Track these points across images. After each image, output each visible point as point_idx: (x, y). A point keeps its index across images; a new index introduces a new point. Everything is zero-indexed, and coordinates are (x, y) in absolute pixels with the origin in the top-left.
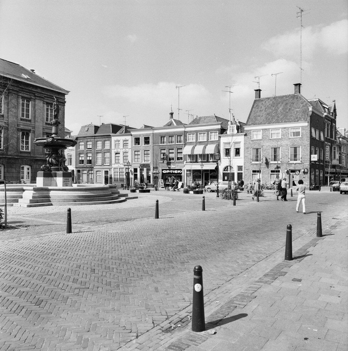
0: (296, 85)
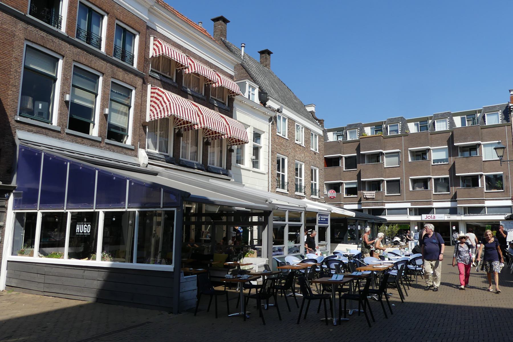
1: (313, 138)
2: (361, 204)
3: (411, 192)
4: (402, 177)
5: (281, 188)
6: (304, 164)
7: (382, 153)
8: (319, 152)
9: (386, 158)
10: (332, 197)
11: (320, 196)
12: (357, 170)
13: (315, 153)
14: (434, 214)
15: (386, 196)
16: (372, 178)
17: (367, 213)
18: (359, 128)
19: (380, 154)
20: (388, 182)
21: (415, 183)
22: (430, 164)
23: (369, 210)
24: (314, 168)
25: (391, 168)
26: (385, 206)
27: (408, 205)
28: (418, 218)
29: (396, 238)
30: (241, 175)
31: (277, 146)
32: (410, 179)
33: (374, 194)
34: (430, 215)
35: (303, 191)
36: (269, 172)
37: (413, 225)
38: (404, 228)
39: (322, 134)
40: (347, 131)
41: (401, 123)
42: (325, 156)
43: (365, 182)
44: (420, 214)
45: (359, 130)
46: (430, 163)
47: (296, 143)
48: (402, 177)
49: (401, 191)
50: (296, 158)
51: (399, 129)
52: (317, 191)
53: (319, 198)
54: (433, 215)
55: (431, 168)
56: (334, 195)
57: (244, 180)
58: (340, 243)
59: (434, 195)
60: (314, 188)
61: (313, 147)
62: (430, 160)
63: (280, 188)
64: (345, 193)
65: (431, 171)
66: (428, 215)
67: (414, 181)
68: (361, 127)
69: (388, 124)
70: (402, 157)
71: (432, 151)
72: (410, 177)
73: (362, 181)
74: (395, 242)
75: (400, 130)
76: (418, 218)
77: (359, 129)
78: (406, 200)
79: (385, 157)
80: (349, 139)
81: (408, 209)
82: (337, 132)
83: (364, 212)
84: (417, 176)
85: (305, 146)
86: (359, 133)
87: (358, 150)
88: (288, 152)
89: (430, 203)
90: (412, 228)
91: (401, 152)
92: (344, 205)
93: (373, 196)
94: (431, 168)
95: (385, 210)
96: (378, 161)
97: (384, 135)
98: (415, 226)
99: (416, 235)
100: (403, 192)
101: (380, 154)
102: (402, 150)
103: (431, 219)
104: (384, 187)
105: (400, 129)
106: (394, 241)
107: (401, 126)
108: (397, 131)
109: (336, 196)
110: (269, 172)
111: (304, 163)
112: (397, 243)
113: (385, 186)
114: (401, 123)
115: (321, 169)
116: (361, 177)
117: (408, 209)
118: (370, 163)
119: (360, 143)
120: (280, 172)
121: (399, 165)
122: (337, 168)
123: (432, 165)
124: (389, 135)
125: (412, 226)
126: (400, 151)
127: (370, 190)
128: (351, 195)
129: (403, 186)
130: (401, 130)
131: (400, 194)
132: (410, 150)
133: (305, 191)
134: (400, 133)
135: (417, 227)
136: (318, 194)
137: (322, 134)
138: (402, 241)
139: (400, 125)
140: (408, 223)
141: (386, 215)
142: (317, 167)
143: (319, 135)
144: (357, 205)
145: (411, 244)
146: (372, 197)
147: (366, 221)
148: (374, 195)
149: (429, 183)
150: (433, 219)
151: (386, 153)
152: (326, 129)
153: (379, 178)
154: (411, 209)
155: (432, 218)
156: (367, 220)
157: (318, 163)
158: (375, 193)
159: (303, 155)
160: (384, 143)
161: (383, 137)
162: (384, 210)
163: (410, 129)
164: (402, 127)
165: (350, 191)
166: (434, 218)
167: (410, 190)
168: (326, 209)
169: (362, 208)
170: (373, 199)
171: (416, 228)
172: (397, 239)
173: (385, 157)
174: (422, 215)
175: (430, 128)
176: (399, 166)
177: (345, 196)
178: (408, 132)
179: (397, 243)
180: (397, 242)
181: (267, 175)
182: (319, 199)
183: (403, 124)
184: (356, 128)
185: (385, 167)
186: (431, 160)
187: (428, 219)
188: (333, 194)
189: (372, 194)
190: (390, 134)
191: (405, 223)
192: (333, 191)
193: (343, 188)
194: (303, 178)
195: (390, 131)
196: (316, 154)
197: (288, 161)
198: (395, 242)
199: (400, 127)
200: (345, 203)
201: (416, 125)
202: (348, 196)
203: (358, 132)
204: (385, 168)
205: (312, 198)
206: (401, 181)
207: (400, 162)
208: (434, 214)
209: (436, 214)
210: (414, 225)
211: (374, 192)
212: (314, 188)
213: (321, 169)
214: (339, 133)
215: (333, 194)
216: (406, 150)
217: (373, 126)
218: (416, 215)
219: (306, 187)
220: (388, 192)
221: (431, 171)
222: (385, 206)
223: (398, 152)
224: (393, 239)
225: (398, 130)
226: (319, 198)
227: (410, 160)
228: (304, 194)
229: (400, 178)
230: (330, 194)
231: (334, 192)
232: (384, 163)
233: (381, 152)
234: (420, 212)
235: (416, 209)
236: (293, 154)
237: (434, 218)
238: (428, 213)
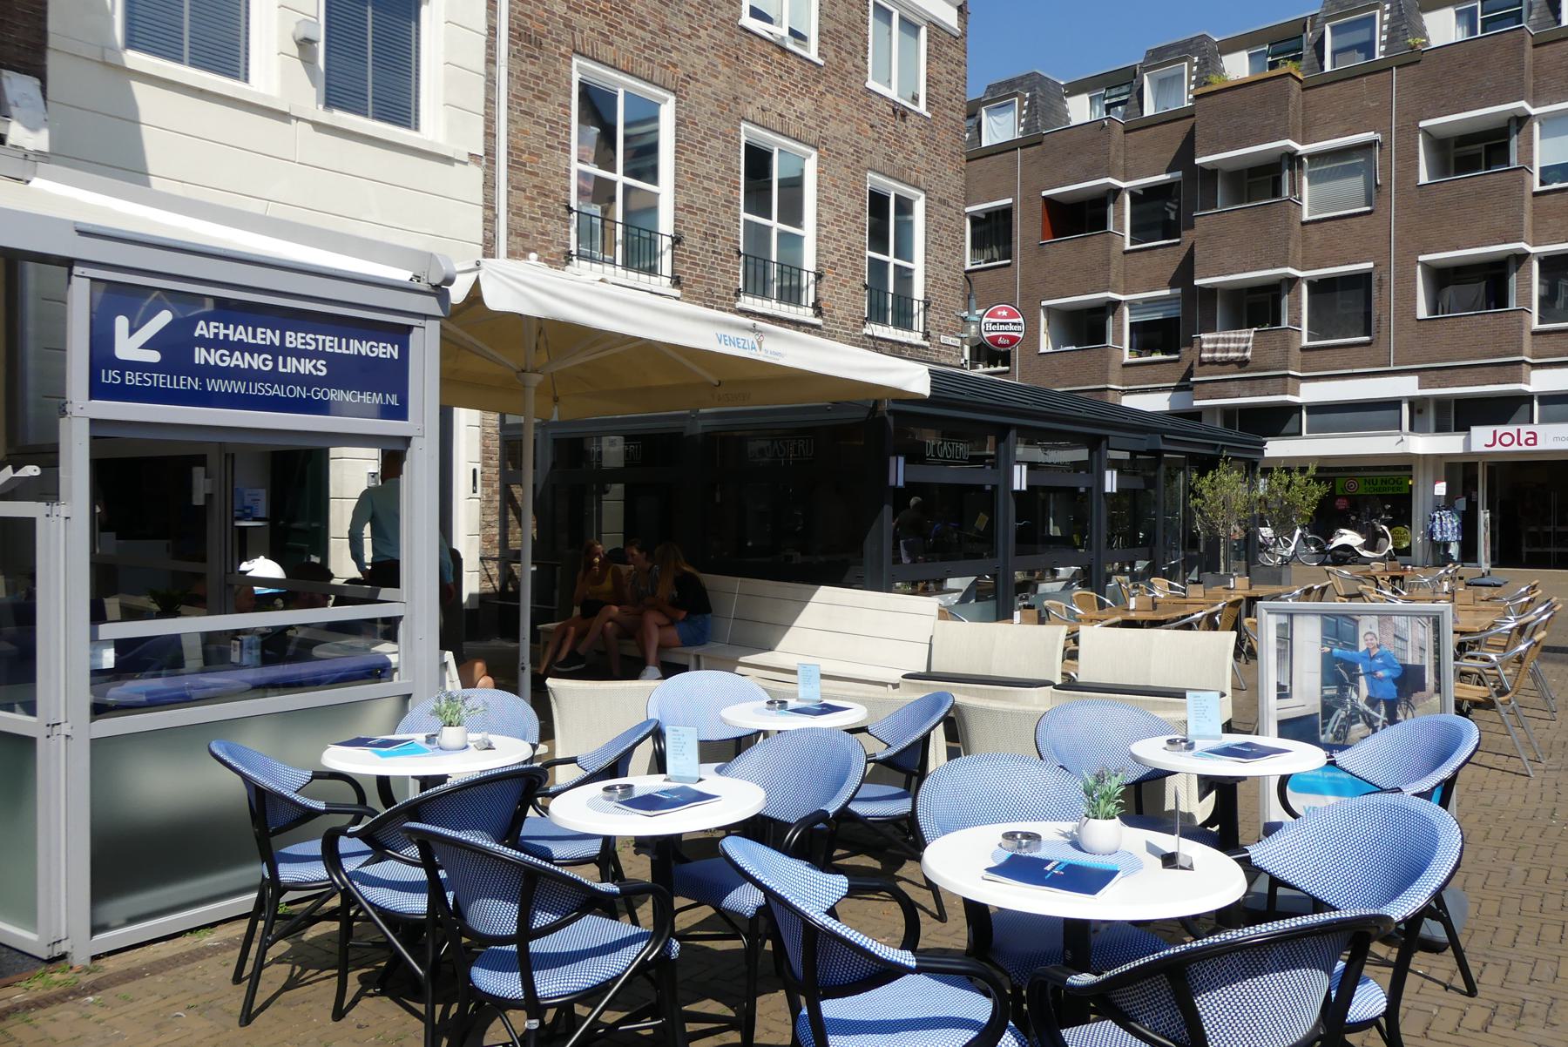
1: (890, 33)
2: (1192, 389)
3: (1422, 323)
4: (1382, 262)
5: (619, 261)
6: (814, 154)
7: (1292, 159)
8: (928, 109)
9: (1310, 183)
10: (1000, 341)
11: (932, 333)
12: (1178, 244)
13: (901, 113)
14: (1531, 421)
15: (1303, 350)
16: (1245, 272)
17: (1219, 424)
18: (1196, 59)
19: (1286, 163)
20: (1317, 287)
21: (1447, 285)
22: (1522, 183)
23: (1228, 412)
24: (893, 188)
25: (1333, 223)
26: (1296, 394)
27: (1407, 386)
28: (1450, 444)
29: (1342, 535)
30: (137, 122)
31: (570, 13)
32: (1419, 267)
33: (1248, 340)
34: (1512, 429)
35: (809, 296)
36: (490, 153)
37: (1425, 476)
38: (1384, 489)
39: (956, 27)
40: (1145, 75)
41: (1388, 7)
42: (1045, 193)
43: (1210, 292)
44: (1463, 427)
45: (1195, 68)
46: (1527, 181)
47: (747, 31)
48: (1382, 262)
49: (1374, 324)
50: (750, 111)
51: (1380, 38)
52: (917, 307)
53: (927, 344)
54: (1525, 428)
55: (1528, 204)
56: (1011, 328)
57: (157, 149)
58: (837, 578)
59: (1535, 333)
60: (1484, 516)
61: (889, 81)
62: (1525, 169)
63: (613, 263)
64: (1131, 347)
65: (1527, 219)
66: (1501, 429)
67: (1441, 277)
68: (1206, 53)
69: (1328, 19)
70: (1386, 168)
71: (1536, 126)
72: (1422, 258)
73: (1200, 288)
74: (1339, 553)
75: (1381, 43)
76: (1450, 444)
77: (1197, 64)
78: (1395, 365)
79: (1305, 180)
80: (1149, 110)
81: (1405, 408)
82: (1107, 89)
83: (1206, 421)
84: (1458, 248)
85: (820, 62)
86: (1194, 78)
87: (1188, 148)
88: (675, 66)
89: (1514, 370)
90: (1420, 489)
91: (1381, 145)
92: (1124, 398)
93: (1245, 350)
94: (1528, 204)
95: (1296, 416)
96: (1277, 192)
97: (1306, 72)
98: (1436, 482)
99: (1438, 521)
100: (1383, 330)
101: (1286, 163)
102: (1387, 133)
103: (1515, 447)
104: (1300, 309)
105: (1384, 38)
106: (1332, 547)
107: (1388, 22)
108: (1368, 48)
109: (1021, 335)
110: (490, 153)
111: (816, 147)
112: (1346, 558)
113: (1300, 304)
114: (1391, 8)
115: (943, 202)
116: (1197, 269)
117: (1405, 408)
118: (1242, 203)
119: (1193, 127)
120: (613, 170)
121: (1370, 205)
122: (1094, 241)
123: (1536, 194)
124: (1328, 68)
125: (1418, 484)
126: (1378, 136)
127: (1237, 326)
128: (1153, 351)
129: (1385, 303)
130: (1388, 43)
131: (1367, 338)
132: (1425, 131)
133: (817, 300)
134: (1381, 53)
135: (1444, 484)
136: (918, 322)
137: (956, 27)
138: (1371, 545)
139: (1387, 17)
140: (1404, 466)
141: (1300, 433)
142: (916, 186)
143: (930, 22)
144: (1168, 395)
145: (1286, 639)
146: (1241, 355)
147: (1099, 444)
148: (1250, 344)
149: (1513, 280)
150: (1525, 448)
151: (1312, 157)
152: (1062, 83)
153: (1274, 267)
154: (1417, 405)
155: (1522, 442)
156: (1107, 437)
157: (922, 164)
158: (1252, 335)
159: (805, 105)
160: (1304, 107)
161: (1300, 81)
162: (1290, 417)
163: (1429, 32)
164: (1394, 25)
165: (1150, 336)
166: (1531, 442)
167: (1419, 317)
168: (403, 276)
169: (1196, 403)
170: (1242, 364)
171: (1441, 489)
172: (1350, 538)
173: (1305, 180)
174: (1474, 429)
175: (1532, 17)
176: (1368, 208)
177: (1127, 357)
178: (1422, 44)
179: (1347, 558)
180: (1348, 554)
181: (476, 174)
182: (926, 348)
183: (1400, 10)
184: (1184, 59)
185: (1306, 217)
186: (1532, 167)
187: (1498, 448)
188: (1005, 324)
189: (1240, 340)
190: (1334, 65)
191: (1387, 468)
192: (1006, 309)
193: (1121, 325)
194: (809, 230)
195: (1334, 53)
196: (904, 116)
197: (677, 118)
198: (1339, 553)
199: (1385, 28)
200: (1126, 388)
201: (1465, 18)
202: (1140, 356)
203: (1190, 73)
204: (1304, 224)
205: (872, 337)
206: (1375, 278)
207: (1374, 192)
208: (1531, 421)
209: (1542, 421)
210: (1430, 478)
211: (1249, 334)
212: (1484, 516)
213: (943, 202)
214: (1114, 92)
215: (1005, 324)
216: (1408, 131)
217: (1263, 44)
218: (1441, 428)
219: (829, 276)
220: (1316, 329)
221: (1527, 219)
222: (1296, 394)
223: (1369, 146)
224: (1329, 536)
225: (1372, 43)
226: (927, 344)
227: (1424, 178)
228: (810, 311)
229: (1370, 265)
230: (990, 327)
231: (1012, 315)
232: (1300, 200)
233: (1288, 153)
234: (1462, 414)
235: (1441, 403)
236: (720, 84)
237: (1531, 442)
238: (1504, 422)
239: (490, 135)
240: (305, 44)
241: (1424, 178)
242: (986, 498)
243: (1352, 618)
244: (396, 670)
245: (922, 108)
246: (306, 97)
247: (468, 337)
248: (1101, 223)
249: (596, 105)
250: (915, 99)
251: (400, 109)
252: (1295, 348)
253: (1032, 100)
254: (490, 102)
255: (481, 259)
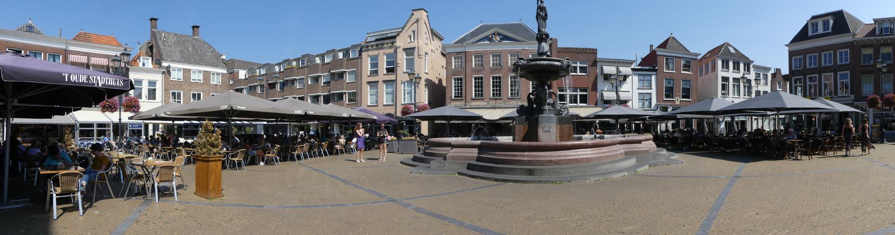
0: (151, 19)
7: (296, 79)
104: (346, 98)
159: (201, 88)
227: (310, 83)
239: (162, 99)
240: (146, 96)
241: (310, 83)
242: (185, 128)
243: (227, 150)
244: (306, 113)
245: (221, 84)
246: (146, 100)
247: (521, 38)
248: (275, 87)
249: (174, 94)
250: (219, 83)
251: (154, 99)
252: (346, 104)
253: (334, 54)
254: (162, 96)
255: (443, 42)
